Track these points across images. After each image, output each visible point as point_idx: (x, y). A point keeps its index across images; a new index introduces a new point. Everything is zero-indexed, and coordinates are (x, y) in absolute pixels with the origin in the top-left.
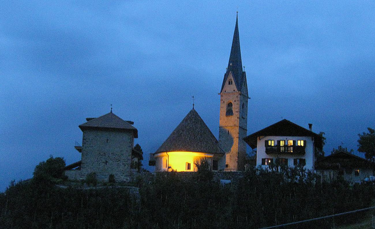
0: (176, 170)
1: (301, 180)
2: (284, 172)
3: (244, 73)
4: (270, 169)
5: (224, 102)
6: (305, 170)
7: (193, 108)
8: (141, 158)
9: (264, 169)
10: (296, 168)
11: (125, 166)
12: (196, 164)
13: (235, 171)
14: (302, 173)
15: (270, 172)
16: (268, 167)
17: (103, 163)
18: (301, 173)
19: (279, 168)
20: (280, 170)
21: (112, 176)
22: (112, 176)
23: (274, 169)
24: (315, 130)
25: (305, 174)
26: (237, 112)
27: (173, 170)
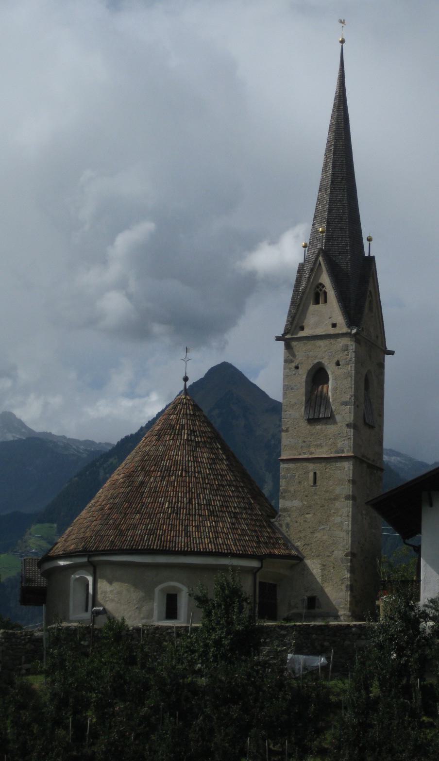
3: (371, 260)
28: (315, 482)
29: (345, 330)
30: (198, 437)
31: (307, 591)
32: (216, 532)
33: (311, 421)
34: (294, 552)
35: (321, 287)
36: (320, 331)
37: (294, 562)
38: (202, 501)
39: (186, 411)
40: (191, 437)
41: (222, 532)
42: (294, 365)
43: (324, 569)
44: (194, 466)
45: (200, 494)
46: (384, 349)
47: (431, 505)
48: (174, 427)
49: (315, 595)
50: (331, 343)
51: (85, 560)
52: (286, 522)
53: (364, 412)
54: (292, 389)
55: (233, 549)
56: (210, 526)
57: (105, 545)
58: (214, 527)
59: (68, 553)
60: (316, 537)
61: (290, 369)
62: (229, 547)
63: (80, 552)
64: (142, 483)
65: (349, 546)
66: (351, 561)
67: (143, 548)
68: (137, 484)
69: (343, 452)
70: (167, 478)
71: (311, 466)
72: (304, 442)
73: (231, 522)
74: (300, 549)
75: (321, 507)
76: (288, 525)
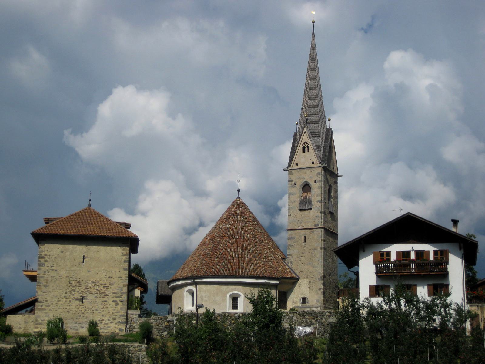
0: (214, 310)
1: (443, 324)
2: (413, 310)
4: (387, 305)
5: (295, 184)
6: (451, 304)
7: (239, 197)
8: (145, 289)
9: (375, 304)
10: (432, 301)
11: (117, 304)
12: (249, 299)
13: (319, 309)
14: (445, 311)
15: (385, 310)
16: (382, 302)
17: (77, 300)
18: (443, 310)
19: (403, 302)
20: (405, 305)
21: (93, 326)
22: (93, 326)
23: (393, 305)
24: (461, 230)
25: (449, 312)
26: (319, 201)
27: (208, 311)
28: (305, 241)
31: (302, 295)
35: (306, 144)
42: (293, 183)
43: (310, 284)
50: (311, 172)
54: (293, 195)
57: (201, 274)
65: (322, 272)
69: (319, 226)
72: (299, 221)
74: (298, 274)
75: (308, 253)
76: (291, 262)
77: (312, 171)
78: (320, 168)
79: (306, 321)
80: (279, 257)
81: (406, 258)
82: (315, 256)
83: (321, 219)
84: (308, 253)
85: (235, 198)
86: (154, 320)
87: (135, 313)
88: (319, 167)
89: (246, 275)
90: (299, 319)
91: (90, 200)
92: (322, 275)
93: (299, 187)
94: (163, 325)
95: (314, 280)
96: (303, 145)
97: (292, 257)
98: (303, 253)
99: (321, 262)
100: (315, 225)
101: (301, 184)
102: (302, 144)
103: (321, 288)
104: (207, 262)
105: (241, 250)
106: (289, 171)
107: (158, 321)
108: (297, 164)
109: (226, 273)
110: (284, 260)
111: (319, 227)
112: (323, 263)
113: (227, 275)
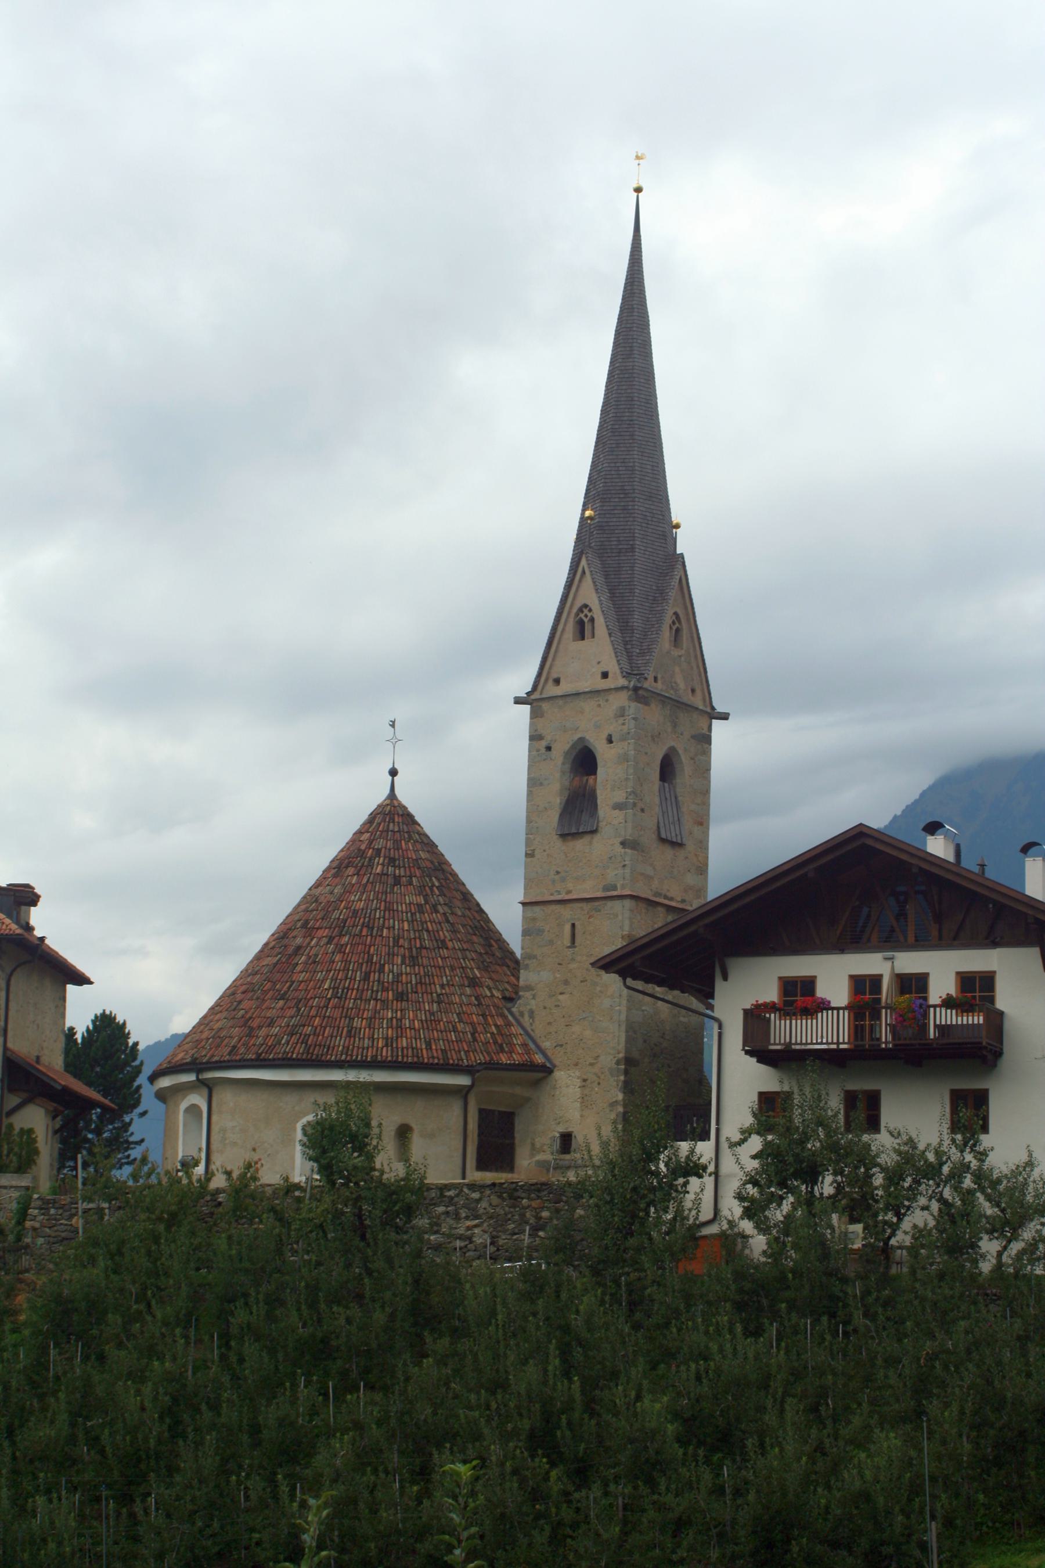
5: (549, 748)
26: (619, 806)
29: (622, 682)
30: (400, 868)
31: (559, 1123)
32: (400, 1027)
33: (564, 836)
34: (539, 1059)
35: (586, 611)
36: (585, 686)
37: (540, 1075)
38: (386, 977)
39: (388, 826)
40: (388, 868)
41: (409, 1028)
43: (584, 1086)
44: (384, 918)
45: (384, 965)
46: (709, 710)
47: (725, 978)
48: (363, 853)
49: (570, 1130)
50: (599, 706)
51: (191, 1077)
52: (529, 1007)
53: (658, 822)
54: (541, 784)
55: (422, 1056)
56: (392, 1019)
57: (223, 1053)
58: (397, 1020)
59: (172, 1067)
60: (573, 1033)
61: (538, 750)
62: (418, 1053)
63: (187, 1064)
64: (299, 948)
65: (622, 1046)
66: (626, 1072)
67: (309, 1057)
68: (290, 950)
69: (615, 888)
70: (335, 940)
71: (567, 913)
72: (558, 873)
73: (429, 1011)
75: (582, 982)
76: (532, 1014)
77: (601, 703)
78: (624, 695)
79: (522, 1215)
80: (493, 996)
81: (977, 994)
82: (601, 992)
83: (624, 866)
84: (582, 982)
85: (380, 795)
86: (41, 1209)
87: (14, 1183)
88: (623, 688)
89: (357, 1057)
90: (497, 1210)
91: (393, 773)
92: (621, 1055)
93: (560, 760)
94: (66, 1225)
95: (596, 1074)
96: (577, 614)
97: (534, 998)
98: (566, 982)
99: (620, 1012)
100: (606, 888)
101: (567, 747)
102: (575, 610)
103: (616, 1101)
104: (248, 1016)
105: (358, 973)
106: (534, 704)
107: (52, 1211)
108: (557, 681)
109: (293, 1053)
110: (509, 1005)
111: (615, 893)
112: (623, 1017)
113: (294, 1059)
